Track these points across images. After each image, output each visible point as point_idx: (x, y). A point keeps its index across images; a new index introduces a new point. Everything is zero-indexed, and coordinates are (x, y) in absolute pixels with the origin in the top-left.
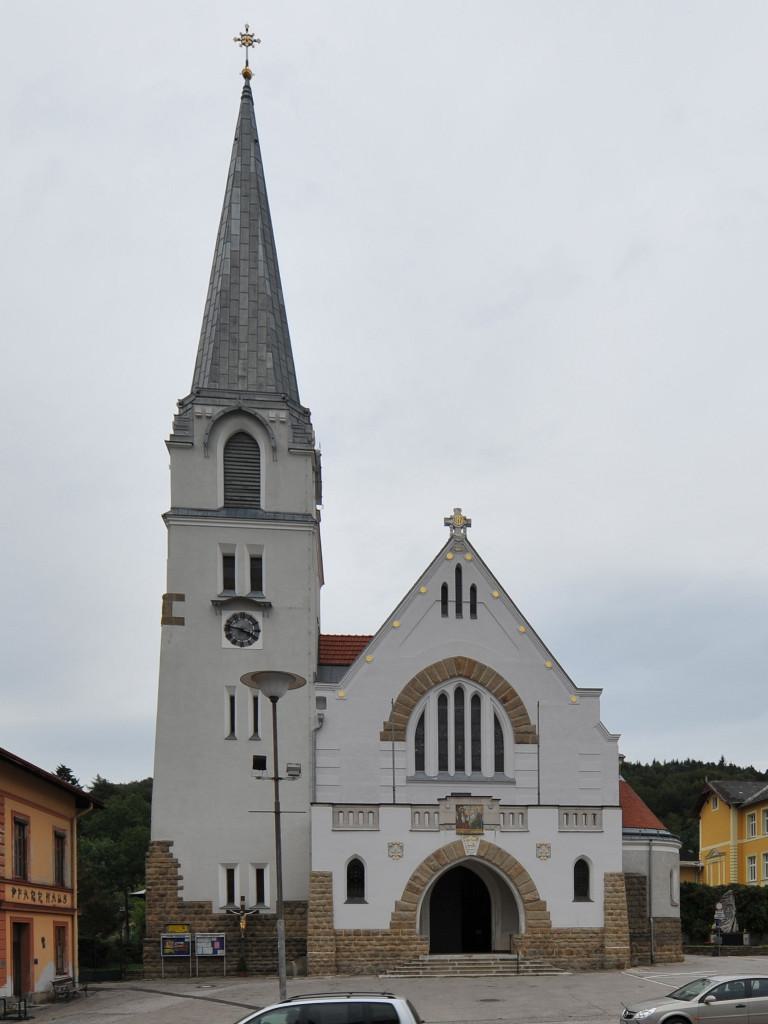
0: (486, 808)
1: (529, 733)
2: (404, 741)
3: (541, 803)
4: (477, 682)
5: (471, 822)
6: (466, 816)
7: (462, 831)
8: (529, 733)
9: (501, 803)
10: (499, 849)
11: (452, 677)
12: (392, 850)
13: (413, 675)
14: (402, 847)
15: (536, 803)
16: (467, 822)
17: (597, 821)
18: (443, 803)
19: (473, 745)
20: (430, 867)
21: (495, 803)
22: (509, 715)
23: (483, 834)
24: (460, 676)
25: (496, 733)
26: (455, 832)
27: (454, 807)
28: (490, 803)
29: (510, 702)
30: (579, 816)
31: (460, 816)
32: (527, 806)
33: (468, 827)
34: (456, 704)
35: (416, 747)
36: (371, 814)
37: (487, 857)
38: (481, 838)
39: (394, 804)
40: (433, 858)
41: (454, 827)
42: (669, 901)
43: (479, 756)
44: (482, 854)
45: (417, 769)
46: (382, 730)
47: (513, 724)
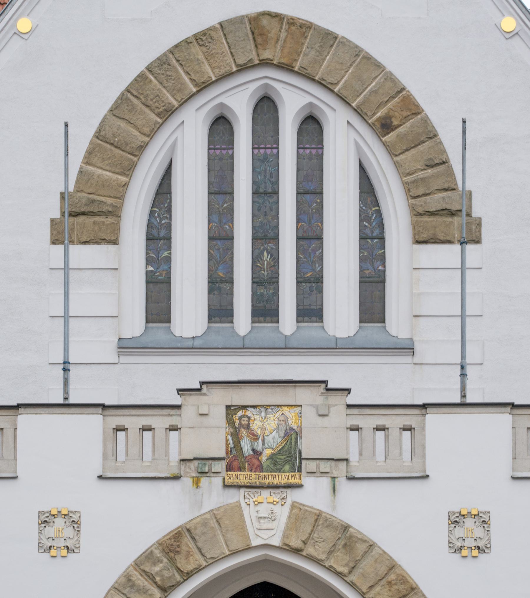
0: (309, 414)
1: (452, 214)
2: (115, 242)
3: (469, 400)
4: (311, 79)
5: (268, 452)
6: (254, 437)
7: (243, 477)
8: (452, 214)
9: (351, 399)
10: (346, 528)
11: (243, 68)
12: (50, 531)
13: (140, 67)
14: (75, 524)
15: (457, 400)
16: (257, 453)
17: (310, 475)
18: (193, 399)
19: (299, 249)
20: (151, 577)
21: (335, 399)
22: (396, 165)
23: (300, 486)
24: (265, 63)
25: (364, 217)
26: (218, 481)
27: (223, 411)
28: (319, 400)
29: (401, 129)
30: (367, 433)
31: (236, 435)
32: (424, 406)
33: (260, 468)
34: (256, 145)
35: (149, 261)
36: (380, 434)
37: (310, 550)
38: (293, 496)
39: (66, 406)
40: (158, 553)
41: (220, 466)
42: (504, 39)
43: (319, 280)
44: (295, 543)
45: (211, 318)
46: (57, 215)
47: (408, 187)
